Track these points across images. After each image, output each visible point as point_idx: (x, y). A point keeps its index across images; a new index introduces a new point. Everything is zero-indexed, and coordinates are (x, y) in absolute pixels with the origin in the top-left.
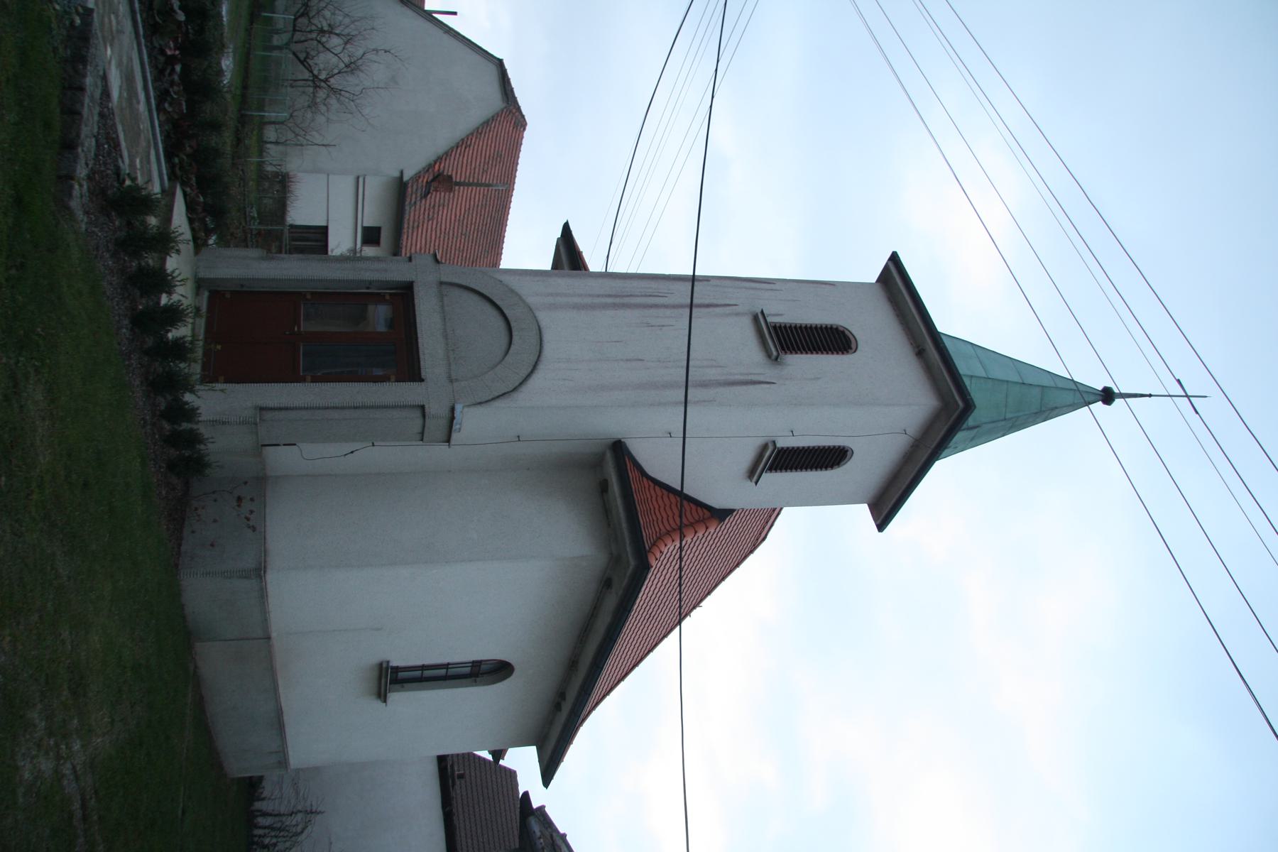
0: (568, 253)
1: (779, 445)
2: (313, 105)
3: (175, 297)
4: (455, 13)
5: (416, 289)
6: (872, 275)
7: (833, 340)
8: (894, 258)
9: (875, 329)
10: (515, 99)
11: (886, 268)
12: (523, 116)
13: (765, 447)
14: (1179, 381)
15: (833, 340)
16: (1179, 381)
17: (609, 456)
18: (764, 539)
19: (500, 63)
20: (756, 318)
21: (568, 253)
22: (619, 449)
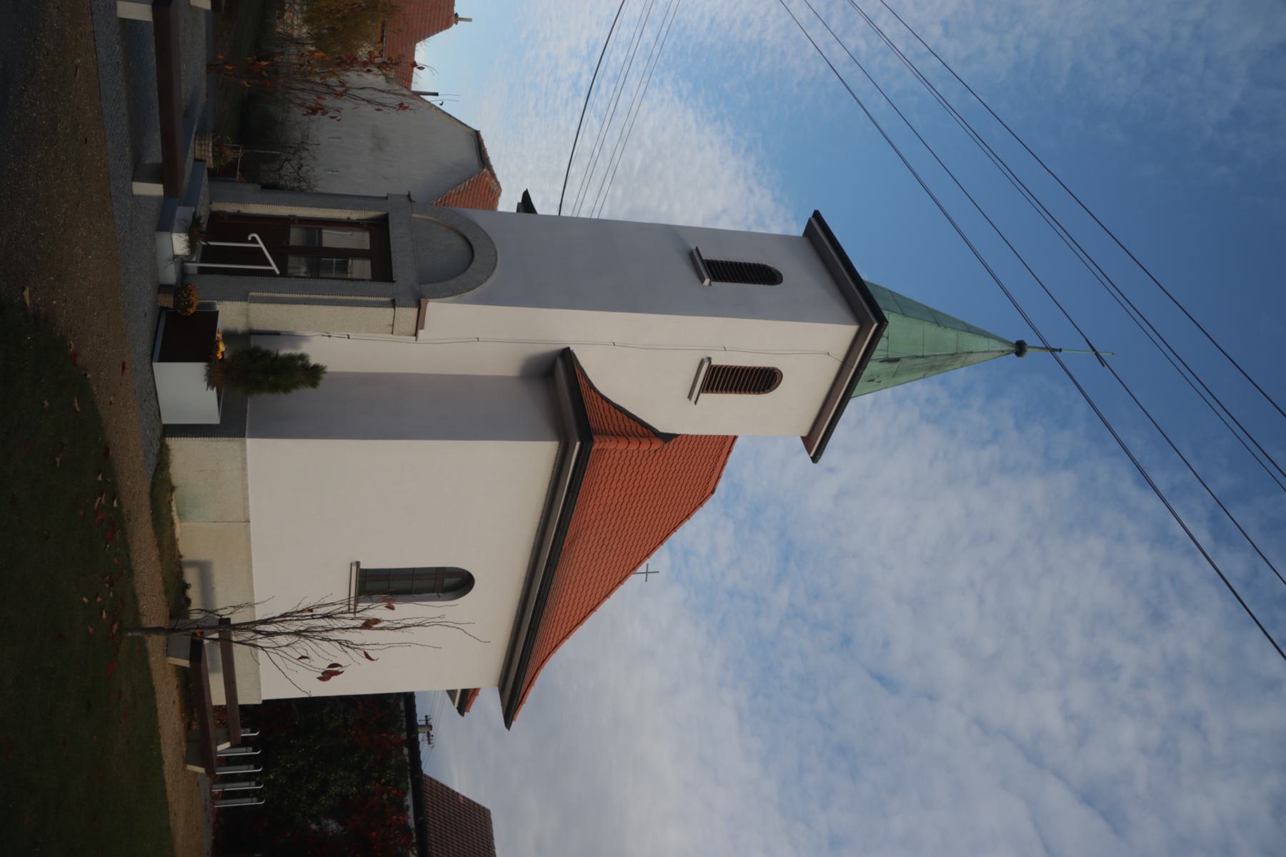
0: (526, 205)
1: (714, 363)
2: (314, 158)
3: (196, 304)
4: (436, 94)
5: (417, 702)
6: (798, 230)
7: (764, 275)
8: (817, 215)
9: (801, 275)
10: (488, 159)
11: (810, 222)
12: (498, 183)
13: (702, 362)
14: (1102, 362)
15: (764, 275)
16: (1102, 362)
17: (560, 365)
18: (713, 492)
19: (477, 134)
20: (691, 254)
21: (526, 205)
22: (566, 355)
